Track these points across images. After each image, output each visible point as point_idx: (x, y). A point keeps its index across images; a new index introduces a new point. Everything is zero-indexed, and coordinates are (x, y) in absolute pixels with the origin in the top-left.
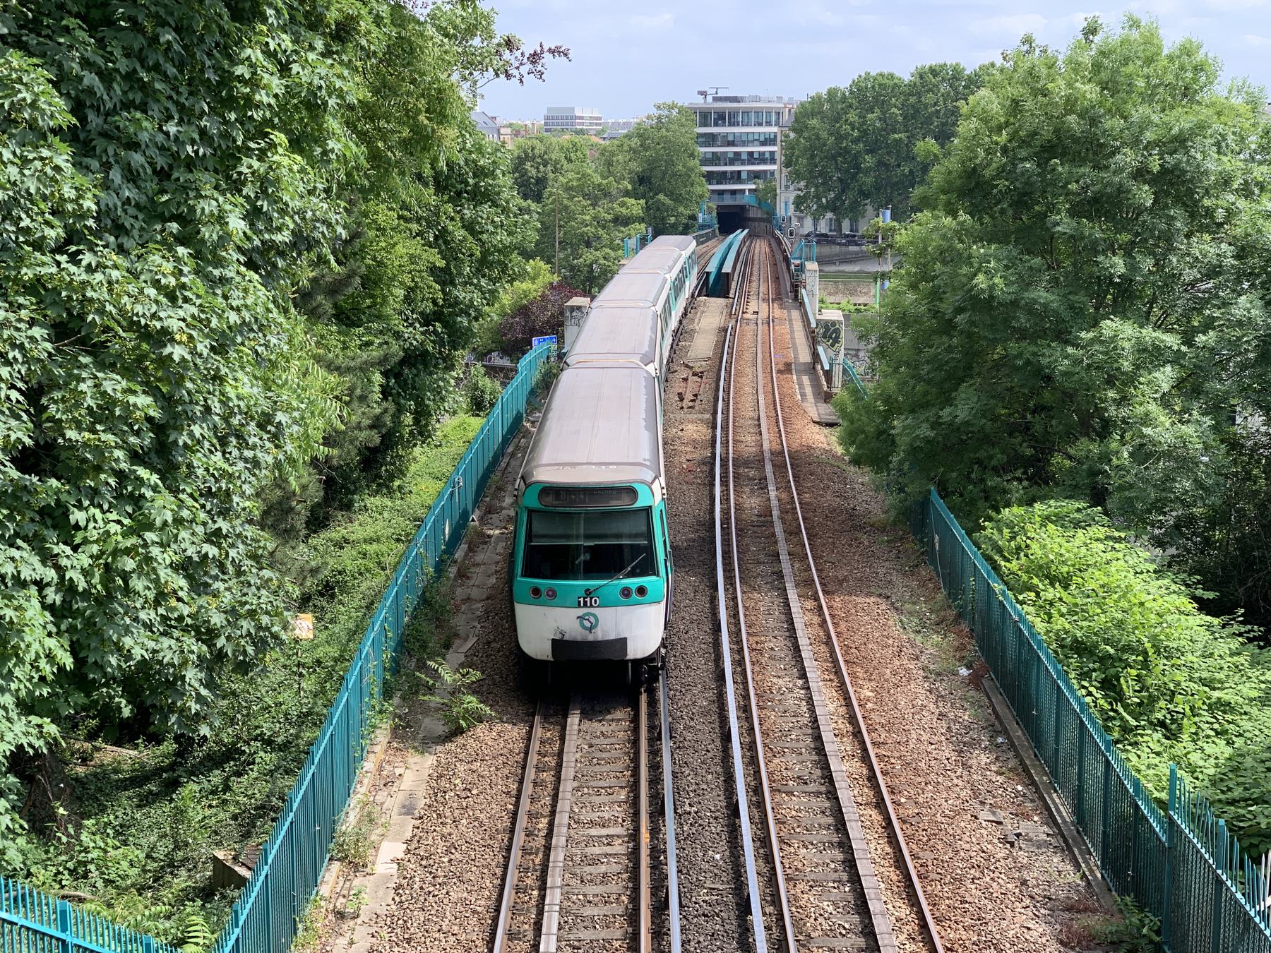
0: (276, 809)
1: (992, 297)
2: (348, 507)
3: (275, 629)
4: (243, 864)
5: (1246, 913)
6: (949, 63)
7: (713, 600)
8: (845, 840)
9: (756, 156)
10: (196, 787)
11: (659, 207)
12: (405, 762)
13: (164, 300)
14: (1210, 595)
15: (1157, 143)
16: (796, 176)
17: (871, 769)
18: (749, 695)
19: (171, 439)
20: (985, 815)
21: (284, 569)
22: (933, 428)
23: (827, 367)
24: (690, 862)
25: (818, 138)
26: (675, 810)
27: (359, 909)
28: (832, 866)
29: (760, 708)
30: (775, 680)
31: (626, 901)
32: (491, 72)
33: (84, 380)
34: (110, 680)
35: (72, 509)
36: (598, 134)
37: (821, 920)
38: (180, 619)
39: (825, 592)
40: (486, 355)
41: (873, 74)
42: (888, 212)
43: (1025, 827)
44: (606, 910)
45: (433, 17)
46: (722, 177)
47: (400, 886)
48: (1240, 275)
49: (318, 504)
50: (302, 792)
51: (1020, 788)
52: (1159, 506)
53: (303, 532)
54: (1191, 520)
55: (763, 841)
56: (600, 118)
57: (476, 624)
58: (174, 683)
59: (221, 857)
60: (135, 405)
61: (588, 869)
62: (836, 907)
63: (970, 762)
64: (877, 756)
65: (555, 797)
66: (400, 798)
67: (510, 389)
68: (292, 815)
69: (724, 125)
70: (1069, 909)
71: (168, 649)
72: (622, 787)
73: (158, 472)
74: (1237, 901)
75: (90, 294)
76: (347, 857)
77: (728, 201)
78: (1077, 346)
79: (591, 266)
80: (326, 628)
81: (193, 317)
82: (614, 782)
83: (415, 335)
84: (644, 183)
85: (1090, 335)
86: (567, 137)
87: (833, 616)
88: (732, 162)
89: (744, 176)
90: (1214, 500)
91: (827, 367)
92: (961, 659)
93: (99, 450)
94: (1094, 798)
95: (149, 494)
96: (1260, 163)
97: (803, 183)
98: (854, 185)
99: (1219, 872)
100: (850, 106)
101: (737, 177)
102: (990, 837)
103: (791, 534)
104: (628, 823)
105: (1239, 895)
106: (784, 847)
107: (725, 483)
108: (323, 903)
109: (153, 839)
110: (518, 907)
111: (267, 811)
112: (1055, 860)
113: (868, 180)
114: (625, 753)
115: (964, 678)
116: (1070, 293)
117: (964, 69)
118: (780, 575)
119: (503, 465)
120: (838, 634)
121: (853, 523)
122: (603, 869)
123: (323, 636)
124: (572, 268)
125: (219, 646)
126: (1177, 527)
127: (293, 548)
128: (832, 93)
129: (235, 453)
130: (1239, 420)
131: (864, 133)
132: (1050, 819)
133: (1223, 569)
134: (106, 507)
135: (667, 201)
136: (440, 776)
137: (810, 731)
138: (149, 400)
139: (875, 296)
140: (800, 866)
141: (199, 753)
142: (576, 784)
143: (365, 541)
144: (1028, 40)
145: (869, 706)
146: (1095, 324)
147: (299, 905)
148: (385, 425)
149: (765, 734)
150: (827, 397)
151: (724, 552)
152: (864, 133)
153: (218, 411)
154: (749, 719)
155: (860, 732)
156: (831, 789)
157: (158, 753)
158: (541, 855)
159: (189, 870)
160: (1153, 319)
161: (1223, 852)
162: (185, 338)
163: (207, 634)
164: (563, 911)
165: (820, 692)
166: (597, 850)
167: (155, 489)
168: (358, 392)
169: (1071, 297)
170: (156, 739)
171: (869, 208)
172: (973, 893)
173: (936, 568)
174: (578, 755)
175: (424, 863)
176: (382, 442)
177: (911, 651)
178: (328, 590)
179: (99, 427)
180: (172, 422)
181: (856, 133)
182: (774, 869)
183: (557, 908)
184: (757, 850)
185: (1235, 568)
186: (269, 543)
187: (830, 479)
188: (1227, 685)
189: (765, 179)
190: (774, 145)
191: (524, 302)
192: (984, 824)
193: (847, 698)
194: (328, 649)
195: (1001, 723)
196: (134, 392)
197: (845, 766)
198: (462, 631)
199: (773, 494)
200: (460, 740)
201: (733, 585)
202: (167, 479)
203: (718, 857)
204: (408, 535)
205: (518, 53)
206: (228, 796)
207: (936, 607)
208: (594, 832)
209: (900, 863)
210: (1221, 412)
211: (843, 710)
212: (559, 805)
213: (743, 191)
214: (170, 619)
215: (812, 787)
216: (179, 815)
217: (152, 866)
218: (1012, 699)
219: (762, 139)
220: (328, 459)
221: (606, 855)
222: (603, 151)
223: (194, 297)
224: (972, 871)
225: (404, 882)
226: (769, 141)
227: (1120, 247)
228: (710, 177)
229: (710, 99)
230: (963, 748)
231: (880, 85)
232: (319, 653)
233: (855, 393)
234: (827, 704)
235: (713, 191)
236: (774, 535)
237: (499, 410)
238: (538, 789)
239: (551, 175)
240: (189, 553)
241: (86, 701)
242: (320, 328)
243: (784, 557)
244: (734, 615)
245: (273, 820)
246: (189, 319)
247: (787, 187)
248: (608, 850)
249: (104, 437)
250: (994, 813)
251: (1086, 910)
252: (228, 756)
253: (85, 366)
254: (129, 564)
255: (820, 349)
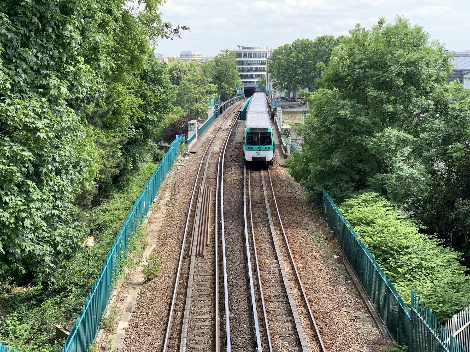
0: (79, 310)
1: (345, 118)
2: (107, 197)
3: (79, 244)
4: (67, 330)
5: (440, 344)
6: (328, 35)
7: (243, 230)
8: (292, 319)
9: (258, 69)
10: (50, 302)
11: (223, 88)
12: (128, 292)
13: (37, 117)
14: (425, 227)
15: (404, 64)
16: (273, 76)
17: (302, 293)
18: (256, 266)
19: (40, 170)
20: (344, 309)
21: (83, 220)
22: (323, 167)
23: (285, 146)
24: (235, 328)
25: (281, 63)
26: (229, 308)
27: (111, 346)
28: (288, 329)
29: (260, 270)
30: (266, 260)
31: (211, 343)
32: (160, 36)
33: (6, 146)
34: (17, 260)
35: (3, 196)
36: (200, 61)
37: (283, 349)
38: (44, 238)
39: (284, 228)
40: (159, 142)
41: (301, 39)
42: (307, 89)
43: (358, 314)
44: (203, 346)
45: (139, 17)
46: (246, 77)
47: (126, 338)
48: (436, 111)
49: (96, 196)
50: (89, 302)
51: (356, 299)
52: (406, 196)
53: (90, 206)
54: (418, 201)
55: (262, 320)
56: (201, 55)
57: (155, 240)
58: (40, 262)
59: (59, 328)
60: (25, 155)
61: (196, 331)
62: (289, 344)
63: (338, 290)
64: (304, 288)
65: (184, 304)
66: (126, 305)
67: (168, 153)
68: (85, 311)
69: (246, 58)
70: (375, 344)
71: (38, 249)
72: (209, 300)
73: (36, 182)
74: (436, 340)
75: (9, 114)
76: (106, 327)
77: (248, 85)
78: (375, 137)
79: (198, 109)
80: (99, 242)
81: (48, 123)
82: (206, 298)
83: (132, 133)
84: (217, 79)
85: (381, 134)
86: (189, 62)
87: (287, 237)
88: (249, 71)
89: (254, 76)
90: (426, 194)
91: (285, 146)
92: (335, 252)
93: (11, 172)
94: (383, 302)
95: (32, 190)
96: (443, 71)
97: (276, 79)
98: (295, 80)
99: (430, 329)
100: (293, 51)
101: (251, 76)
102: (346, 318)
103: (272, 206)
104: (212, 313)
105: (437, 338)
106: (270, 322)
107: (247, 188)
108: (97, 344)
109: (33, 321)
110: (170, 345)
111: (76, 310)
112: (370, 326)
113: (299, 78)
114: (211, 287)
115: (336, 259)
116: (373, 118)
117: (334, 38)
118: (268, 222)
119: (165, 182)
120: (289, 243)
121: (294, 202)
122: (202, 331)
123: (97, 245)
124: (192, 110)
125: (58, 249)
126: (413, 203)
127: (86, 212)
128: (286, 46)
129: (65, 176)
130: (435, 165)
131: (298, 61)
132: (368, 311)
133: (430, 219)
134: (16, 195)
135: (226, 85)
136: (141, 297)
137: (279, 279)
138: (30, 154)
139: (302, 120)
140: (275, 329)
141: (51, 289)
142: (192, 299)
143: (114, 210)
144: (358, 26)
145: (301, 269)
146: (382, 131)
147: (88, 345)
148: (121, 166)
149: (262, 280)
150: (285, 157)
151: (247, 213)
152: (298, 61)
153: (58, 161)
154: (256, 274)
155: (298, 279)
156: (287, 300)
157: (35, 289)
158: (179, 326)
159: (47, 333)
160: (404, 127)
161: (431, 322)
162: (44, 131)
163: (54, 245)
164: (187, 347)
165: (283, 264)
166: (200, 324)
167: (34, 188)
168: (111, 154)
169: (373, 119)
170: (35, 284)
171: (300, 88)
172: (339, 338)
173: (325, 219)
174: (193, 288)
175: (135, 329)
176: (120, 173)
177: (316, 249)
178: (100, 228)
179: (11, 164)
180: (40, 164)
181: (295, 61)
182: (266, 330)
183: (185, 345)
184: (259, 323)
185: (434, 218)
186: (77, 210)
187: (286, 186)
188: (431, 260)
189: (262, 77)
190: (265, 65)
191: (173, 122)
192: (343, 313)
193: (293, 267)
194: (99, 250)
195: (350, 276)
196: (24, 151)
197: (292, 292)
198: (149, 243)
199: (265, 192)
200: (149, 283)
201: (250, 225)
202: (39, 185)
203: (245, 326)
204: (130, 207)
205: (170, 29)
206: (61, 305)
207: (325, 233)
208: (199, 317)
209: (312, 327)
210: (428, 162)
211: (291, 271)
212: (186, 307)
213: (254, 82)
214: (40, 238)
215: (280, 300)
216: (44, 312)
217: (33, 331)
218: (354, 267)
219: (261, 63)
220: (100, 178)
221: (203, 326)
222: (202, 67)
223: (48, 117)
224: (339, 330)
225: (128, 336)
226: (263, 63)
227: (391, 101)
228: (241, 76)
229: (241, 48)
230: (336, 284)
231: (304, 44)
232: (96, 251)
233: (296, 155)
234: (285, 268)
235: (243, 82)
236: (265, 207)
237: (164, 162)
238: (178, 301)
239: (182, 76)
240: (47, 213)
241: (8, 268)
242: (97, 131)
243: (269, 215)
244: (251, 236)
245: (78, 314)
246: (46, 124)
247: (270, 80)
248: (204, 323)
249: (12, 168)
250: (347, 309)
251: (381, 344)
252: (62, 290)
253: (6, 141)
254: (24, 215)
255: (282, 139)
